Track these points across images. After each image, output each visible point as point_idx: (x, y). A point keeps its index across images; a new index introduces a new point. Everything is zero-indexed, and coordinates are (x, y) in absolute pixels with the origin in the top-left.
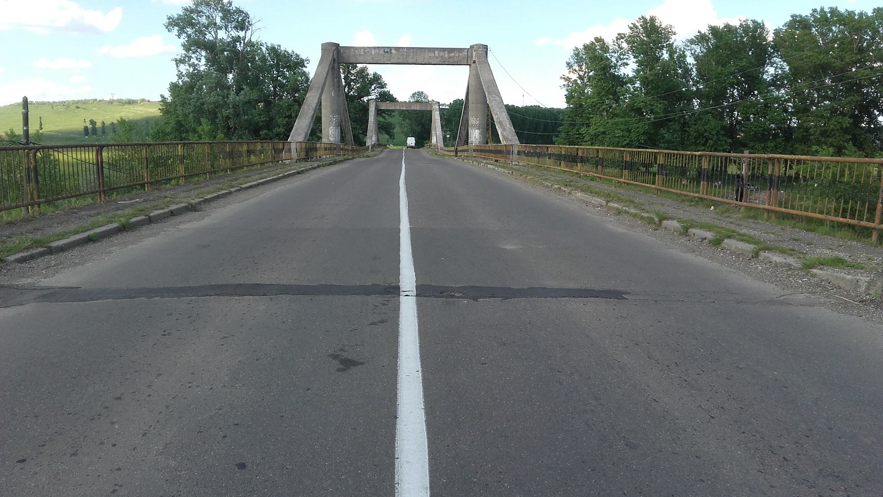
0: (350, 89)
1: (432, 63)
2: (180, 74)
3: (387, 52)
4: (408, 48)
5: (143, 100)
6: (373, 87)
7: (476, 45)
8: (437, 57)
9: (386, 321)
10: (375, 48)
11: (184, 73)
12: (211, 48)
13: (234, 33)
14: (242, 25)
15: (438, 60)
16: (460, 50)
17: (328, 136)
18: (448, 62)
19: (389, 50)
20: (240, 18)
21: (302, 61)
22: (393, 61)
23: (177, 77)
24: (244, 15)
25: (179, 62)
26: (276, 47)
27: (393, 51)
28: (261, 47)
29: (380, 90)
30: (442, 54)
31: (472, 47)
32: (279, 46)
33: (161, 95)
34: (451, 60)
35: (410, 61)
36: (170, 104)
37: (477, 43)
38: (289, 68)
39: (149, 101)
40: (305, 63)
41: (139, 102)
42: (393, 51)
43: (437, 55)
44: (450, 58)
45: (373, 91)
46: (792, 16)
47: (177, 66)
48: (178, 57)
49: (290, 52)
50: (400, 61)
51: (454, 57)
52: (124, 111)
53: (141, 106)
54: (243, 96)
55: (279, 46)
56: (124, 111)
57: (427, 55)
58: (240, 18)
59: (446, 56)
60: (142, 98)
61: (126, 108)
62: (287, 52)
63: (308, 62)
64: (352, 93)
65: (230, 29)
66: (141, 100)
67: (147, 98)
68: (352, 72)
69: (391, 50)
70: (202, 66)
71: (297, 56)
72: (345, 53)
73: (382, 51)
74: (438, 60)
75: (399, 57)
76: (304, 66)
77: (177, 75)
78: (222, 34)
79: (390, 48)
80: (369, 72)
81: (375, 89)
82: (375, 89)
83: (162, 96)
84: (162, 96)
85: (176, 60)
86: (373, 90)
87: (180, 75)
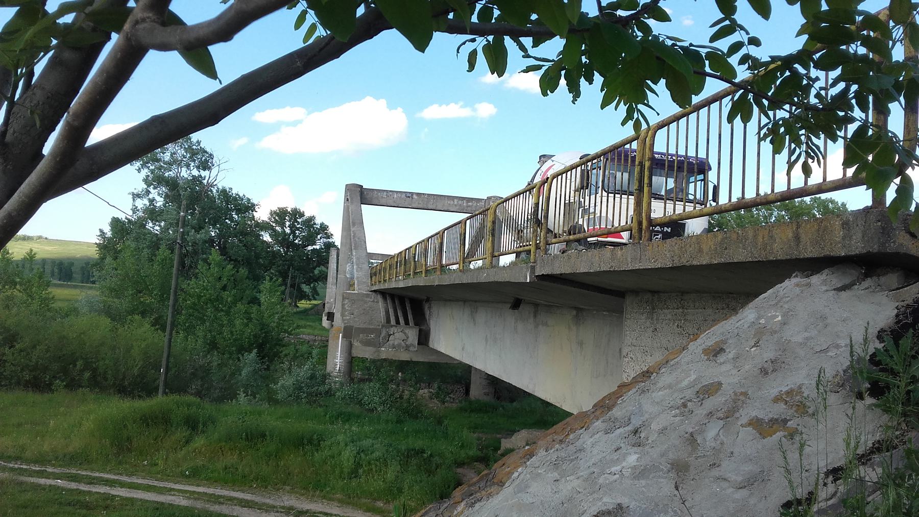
0: (295, 237)
1: (452, 210)
2: (135, 208)
3: (409, 197)
4: (429, 195)
5: (40, 237)
6: (319, 237)
7: (494, 197)
8: (455, 205)
9: (868, 321)
10: (397, 192)
11: (139, 208)
12: (173, 185)
13: (195, 172)
14: (205, 165)
15: (458, 207)
16: (478, 200)
17: (345, 272)
18: (466, 210)
19: (410, 195)
20: (204, 158)
21: (253, 205)
22: (414, 206)
23: (131, 211)
24: (207, 155)
25: (136, 196)
26: (228, 190)
27: (415, 196)
28: (212, 189)
29: (325, 240)
30: (460, 202)
31: (489, 198)
32: (231, 189)
33: (100, 229)
34: (469, 208)
35: (430, 207)
36: (109, 239)
37: (494, 195)
38: (239, 211)
39: (46, 238)
40: (256, 207)
41: (35, 239)
42: (415, 196)
43: (456, 203)
44: (468, 206)
45: (319, 241)
46: (737, 199)
47: (134, 200)
48: (135, 192)
49: (241, 195)
50: (420, 206)
51: (472, 206)
52: (17, 248)
53: (38, 243)
54: (203, 235)
55: (231, 189)
56: (17, 248)
57: (447, 202)
58: (204, 158)
59: (465, 204)
60: (39, 235)
61: (20, 244)
62: (239, 196)
63: (259, 206)
64: (297, 241)
65: (192, 168)
66: (38, 236)
67: (44, 236)
68: (298, 220)
69: (412, 195)
70: (160, 202)
71: (249, 200)
72: (367, 194)
73: (404, 196)
74: (458, 207)
75: (420, 202)
76: (254, 210)
77: (131, 209)
78: (184, 173)
79: (412, 194)
80: (316, 222)
81: (321, 238)
82: (321, 238)
83: (101, 231)
84: (101, 231)
85: (133, 194)
86: (318, 240)
87: (135, 210)
